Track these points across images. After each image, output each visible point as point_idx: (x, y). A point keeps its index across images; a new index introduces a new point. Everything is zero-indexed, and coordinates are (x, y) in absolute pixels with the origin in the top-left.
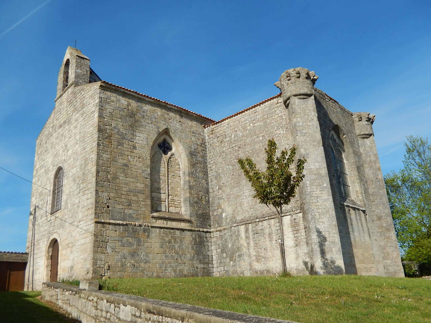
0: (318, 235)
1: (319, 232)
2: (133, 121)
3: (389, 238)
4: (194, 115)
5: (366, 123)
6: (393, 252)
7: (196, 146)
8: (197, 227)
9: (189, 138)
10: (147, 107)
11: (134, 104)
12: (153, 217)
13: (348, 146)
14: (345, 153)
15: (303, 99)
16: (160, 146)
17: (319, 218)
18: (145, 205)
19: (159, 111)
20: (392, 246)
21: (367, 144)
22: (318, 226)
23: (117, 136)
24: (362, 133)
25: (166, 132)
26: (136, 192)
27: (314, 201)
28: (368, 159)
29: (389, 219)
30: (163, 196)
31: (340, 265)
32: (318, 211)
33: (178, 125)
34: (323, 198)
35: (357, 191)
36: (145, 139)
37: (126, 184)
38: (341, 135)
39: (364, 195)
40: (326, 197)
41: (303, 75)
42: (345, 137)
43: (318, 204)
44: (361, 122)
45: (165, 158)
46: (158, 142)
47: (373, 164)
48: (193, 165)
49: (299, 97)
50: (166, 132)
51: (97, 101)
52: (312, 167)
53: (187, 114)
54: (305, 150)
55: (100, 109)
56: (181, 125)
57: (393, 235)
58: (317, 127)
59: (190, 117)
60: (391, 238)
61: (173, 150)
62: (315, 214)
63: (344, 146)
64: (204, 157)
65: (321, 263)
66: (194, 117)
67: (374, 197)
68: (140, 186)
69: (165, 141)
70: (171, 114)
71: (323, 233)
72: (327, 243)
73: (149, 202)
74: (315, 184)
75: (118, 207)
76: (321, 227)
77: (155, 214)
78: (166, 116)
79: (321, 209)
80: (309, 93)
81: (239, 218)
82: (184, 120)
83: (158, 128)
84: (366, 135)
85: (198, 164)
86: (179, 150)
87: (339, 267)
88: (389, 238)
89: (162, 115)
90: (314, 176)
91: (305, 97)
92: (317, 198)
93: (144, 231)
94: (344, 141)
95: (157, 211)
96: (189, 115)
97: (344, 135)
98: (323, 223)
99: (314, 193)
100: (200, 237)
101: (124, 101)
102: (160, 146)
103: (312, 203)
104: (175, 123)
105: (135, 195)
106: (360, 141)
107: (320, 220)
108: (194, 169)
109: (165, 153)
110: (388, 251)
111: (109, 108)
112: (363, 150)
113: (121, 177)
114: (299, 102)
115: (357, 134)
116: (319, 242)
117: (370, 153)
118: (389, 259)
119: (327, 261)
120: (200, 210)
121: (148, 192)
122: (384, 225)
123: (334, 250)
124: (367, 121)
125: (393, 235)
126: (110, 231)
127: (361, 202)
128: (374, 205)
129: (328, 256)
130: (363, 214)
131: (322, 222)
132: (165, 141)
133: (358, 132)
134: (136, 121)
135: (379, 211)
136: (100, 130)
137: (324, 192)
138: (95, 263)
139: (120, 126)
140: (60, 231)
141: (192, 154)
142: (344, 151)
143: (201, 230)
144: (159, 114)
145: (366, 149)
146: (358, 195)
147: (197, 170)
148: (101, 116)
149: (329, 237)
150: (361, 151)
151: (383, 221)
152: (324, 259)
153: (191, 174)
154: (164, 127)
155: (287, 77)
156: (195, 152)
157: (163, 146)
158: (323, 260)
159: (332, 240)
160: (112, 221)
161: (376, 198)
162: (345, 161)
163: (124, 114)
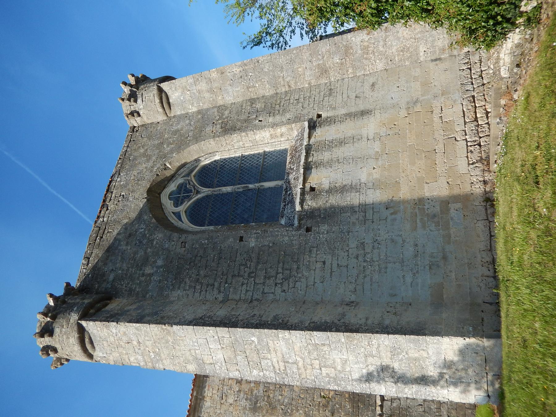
0: (378, 382)
1: (369, 378)
3: (365, 49)
4: (195, 394)
5: (139, 101)
6: (398, 39)
7: (242, 395)
9: (231, 409)
13: (185, 155)
14: (202, 159)
15: (92, 342)
17: (335, 368)
20: (385, 41)
21: (179, 97)
22: (356, 376)
24: (161, 110)
27: (295, 370)
28: (207, 95)
29: (324, 50)
31: (456, 347)
32: (318, 367)
34: (285, 350)
35: (272, 137)
38: (168, 174)
39: (278, 118)
40: (282, 343)
41: (47, 341)
42: (170, 164)
43: (300, 364)
44: (141, 113)
47: (215, 85)
49: (90, 351)
52: (220, 356)
53: (195, 408)
54: (188, 362)
57: (359, 39)
58: (137, 329)
59: (198, 401)
60: (366, 44)
62: (324, 375)
63: (189, 161)
65: (452, 389)
66: (197, 393)
67: (280, 83)
71: (371, 368)
72: (396, 366)
74: (255, 359)
76: (357, 370)
79: (311, 360)
80: (77, 335)
84: (161, 102)
85: (269, 396)
87: (462, 352)
88: (365, 49)
90: (239, 358)
91: (87, 340)
92: (288, 362)
94: (178, 164)
96: (195, 404)
97: (166, 168)
98: (345, 362)
99: (276, 365)
103: (300, 375)
106: (177, 111)
107: (339, 368)
108: (278, 407)
110: (397, 51)
112: (192, 105)
114: (101, 350)
115: (165, 118)
116: (395, 383)
117: (195, 91)
118: (417, 49)
119: (447, 377)
120: (345, 406)
122: (337, 60)
123: (413, 354)
124: (136, 101)
125: (359, 39)
127: (292, 129)
128: (296, 83)
129: (432, 372)
130: (320, 134)
131: (343, 364)
133: (161, 118)
135: (308, 73)
137: (271, 344)
142: (197, 160)
145: (189, 100)
146: (278, 134)
147: (279, 400)
149: (380, 358)
150: (195, 109)
151: (329, 64)
152: (439, 381)
155: (62, 364)
156: (250, 400)
158: (442, 383)
159: (389, 354)
161: (281, 79)
162: (217, 158)
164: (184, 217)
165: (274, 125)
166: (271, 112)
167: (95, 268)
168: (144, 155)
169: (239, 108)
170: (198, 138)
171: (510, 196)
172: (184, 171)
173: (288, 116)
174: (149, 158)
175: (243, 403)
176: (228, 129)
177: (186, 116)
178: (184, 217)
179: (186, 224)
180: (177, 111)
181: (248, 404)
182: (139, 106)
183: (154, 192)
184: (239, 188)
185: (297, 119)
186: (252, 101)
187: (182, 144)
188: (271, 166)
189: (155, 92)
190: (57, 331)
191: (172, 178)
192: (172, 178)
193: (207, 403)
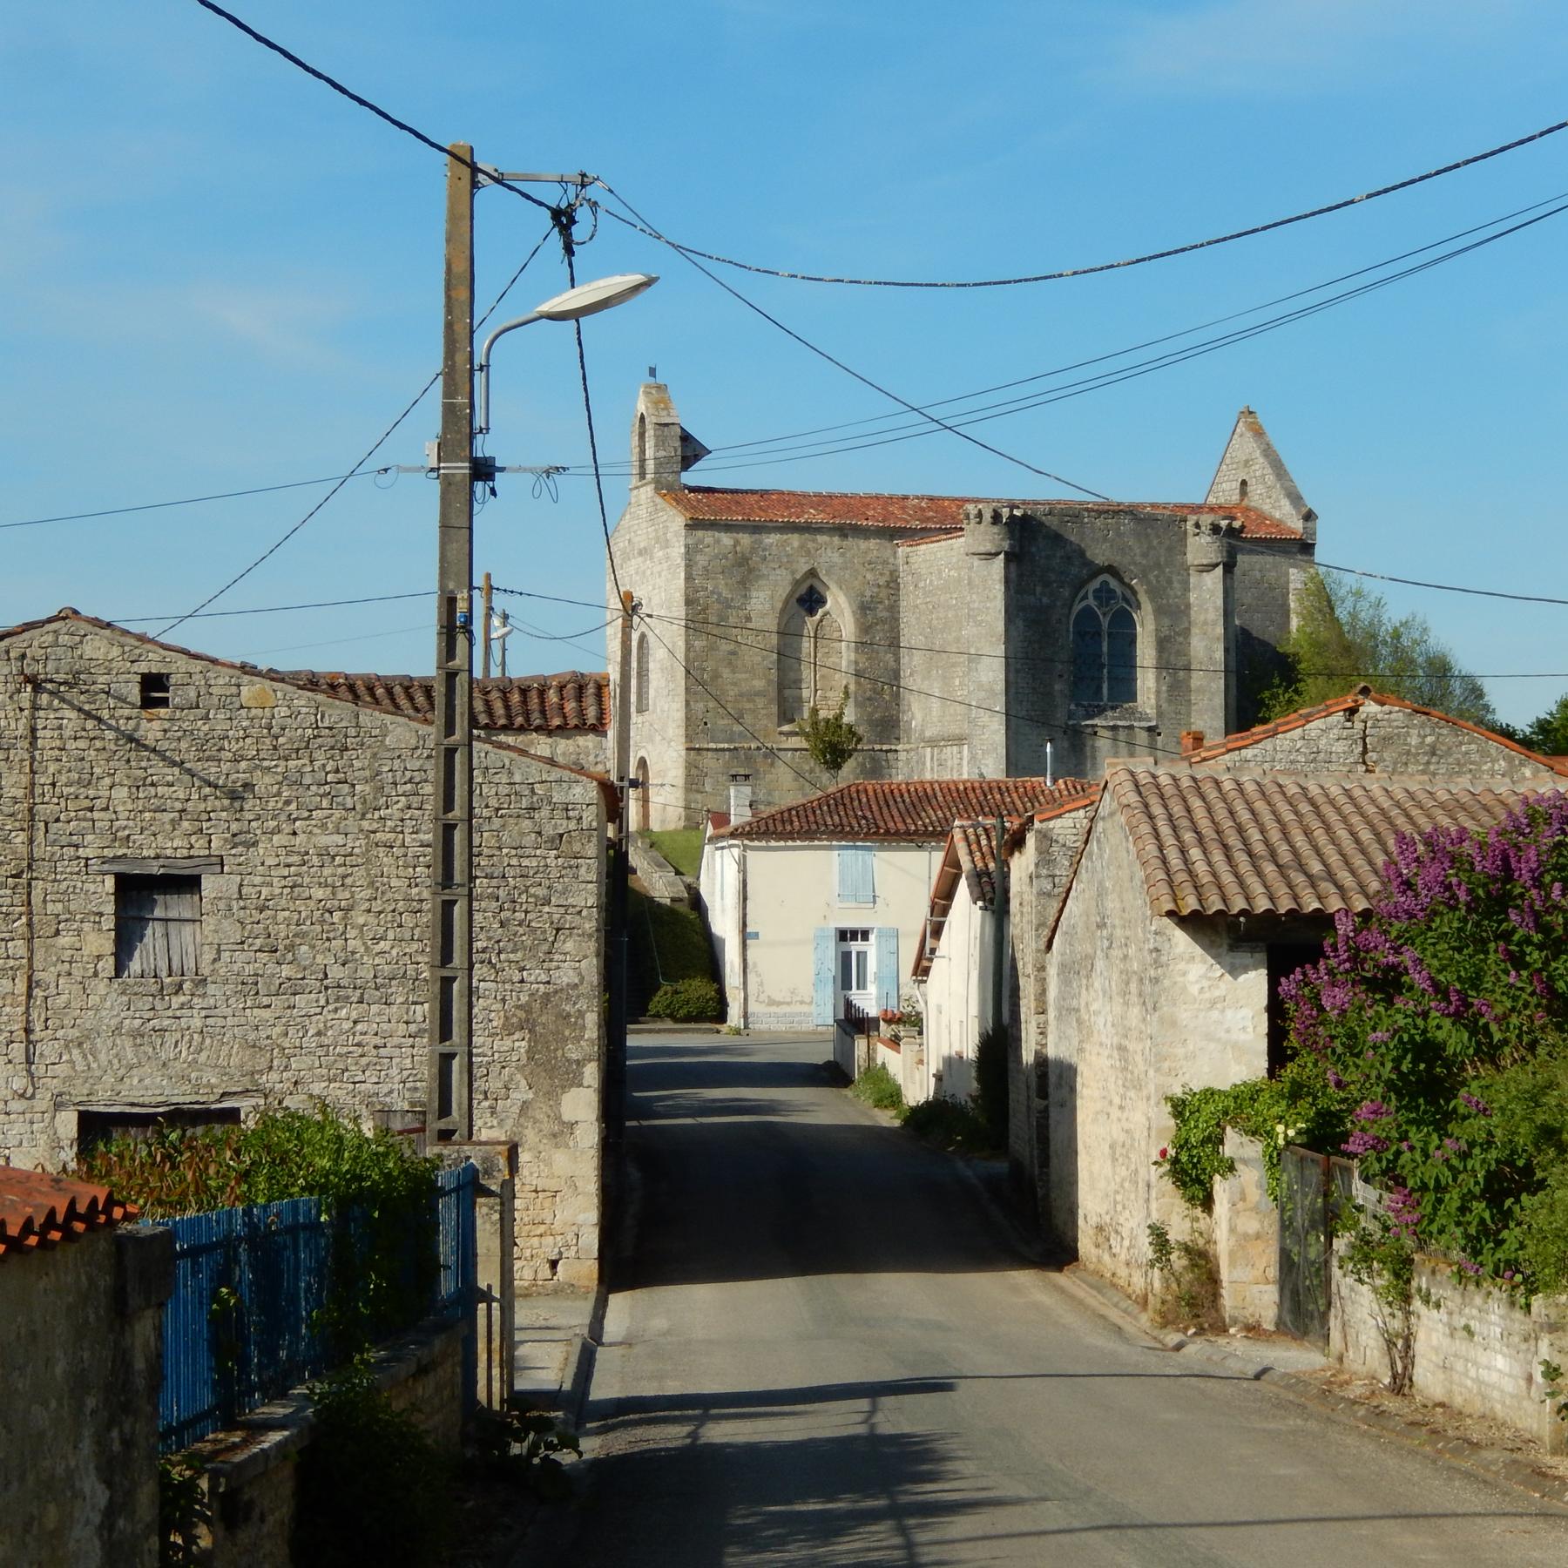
2: (745, 571)
8: (869, 742)
10: (772, 539)
11: (745, 539)
12: (781, 733)
16: (801, 601)
18: (768, 716)
19: (795, 540)
23: (716, 606)
25: (812, 573)
26: (751, 696)
28: (1202, 618)
30: (805, 693)
33: (836, 558)
36: (765, 602)
37: (735, 684)
39: (1164, 695)
41: (987, 516)
45: (811, 622)
46: (797, 595)
48: (865, 628)
50: (812, 573)
51: (683, 550)
55: (687, 566)
56: (842, 555)
61: (828, 606)
64: (894, 609)
68: (759, 684)
69: (812, 589)
70: (822, 539)
73: (774, 709)
75: (721, 722)
77: (786, 728)
78: (810, 545)
81: (928, 734)
82: (850, 542)
83: (793, 573)
86: (840, 608)
89: (802, 547)
93: (766, 756)
95: (792, 721)
100: (873, 759)
101: (726, 539)
102: (801, 601)
104: (829, 554)
105: (749, 701)
109: (812, 612)
111: (701, 560)
113: (726, 673)
121: (773, 693)
126: (708, 761)
132: (812, 589)
134: (750, 571)
136: (689, 602)
138: (687, 808)
139: (722, 586)
140: (650, 747)
141: (864, 608)
143: (877, 747)
144: (796, 544)
148: (689, 578)
153: (860, 645)
154: (806, 568)
157: (810, 599)
160: (713, 746)
163: (728, 564)
164: (1084, 603)
165: (1158, 692)
166: (1171, 688)
167: (1041, 524)
168: (1151, 547)
169: (1184, 652)
170: (1159, 612)
171: (1502, 1109)
172: (1128, 594)
173: (1164, 706)
174: (1145, 555)
175: (868, 593)
176: (1162, 644)
177: (1187, 589)
178: (1084, 603)
179: (1077, 608)
180: (1194, 579)
181: (868, 599)
182: (1206, 539)
183: (1111, 570)
184: (1105, 659)
185: (1160, 714)
186: (1188, 669)
187: (1154, 593)
188: (1125, 690)
189: (1215, 561)
190: (995, 529)
191: (1121, 580)
192: (1121, 580)
193: (863, 544)
